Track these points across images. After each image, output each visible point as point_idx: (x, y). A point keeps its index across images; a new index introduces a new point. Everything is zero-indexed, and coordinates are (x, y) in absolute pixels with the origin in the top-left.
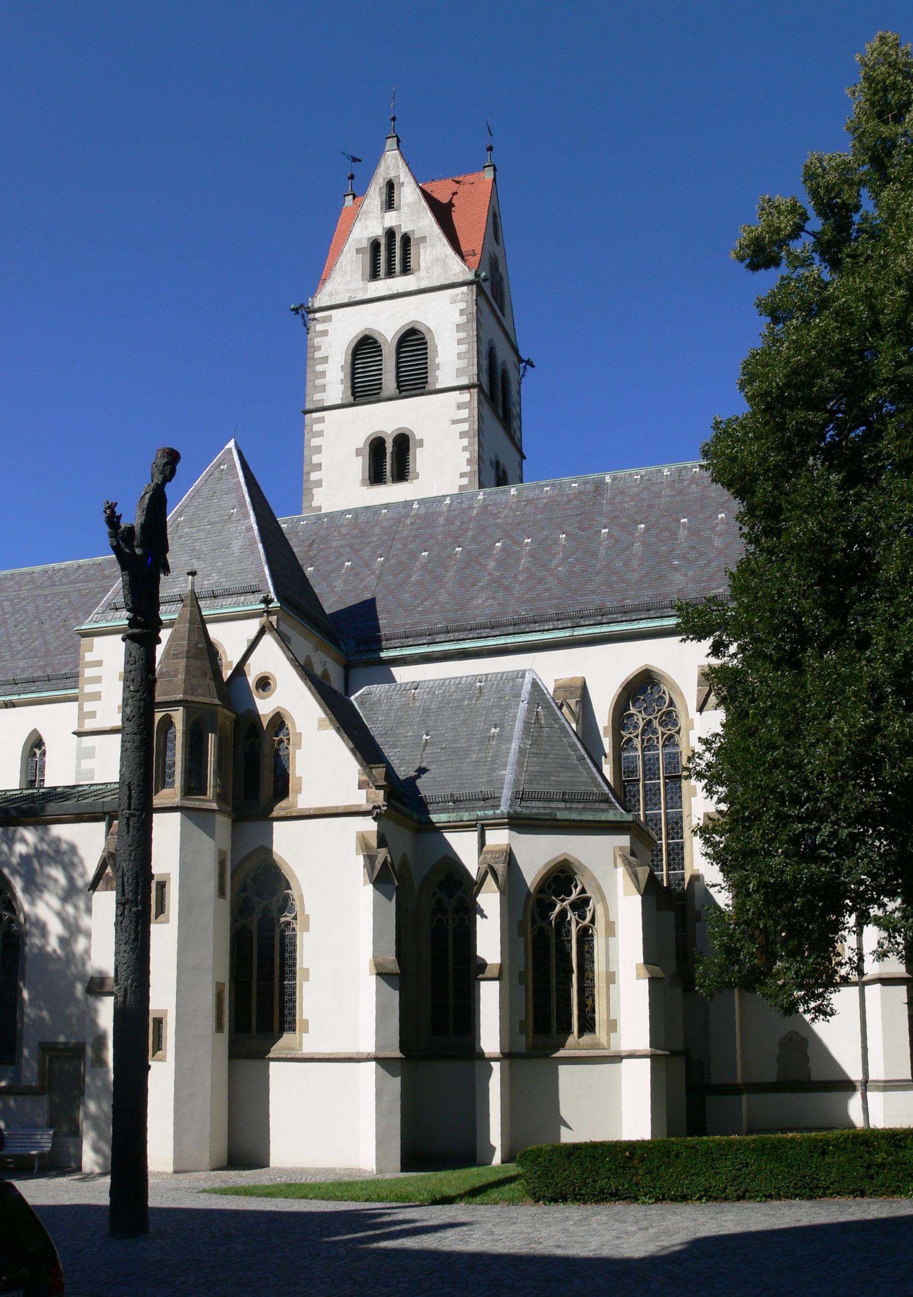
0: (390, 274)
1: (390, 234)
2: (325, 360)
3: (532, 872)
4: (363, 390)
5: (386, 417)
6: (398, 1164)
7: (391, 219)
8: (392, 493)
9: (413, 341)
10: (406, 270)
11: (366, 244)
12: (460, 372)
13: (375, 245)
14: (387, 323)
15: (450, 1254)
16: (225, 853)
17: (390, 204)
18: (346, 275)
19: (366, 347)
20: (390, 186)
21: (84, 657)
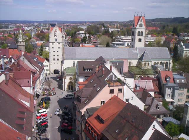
1: (141, 24)
4: (139, 35)
5: (140, 37)
6: (124, 62)
7: (141, 23)
8: (112, 88)
10: (142, 27)
13: (140, 24)
14: (141, 31)
15: (150, 126)
17: (141, 21)
18: (138, 27)
19: (139, 32)
21: (79, 80)
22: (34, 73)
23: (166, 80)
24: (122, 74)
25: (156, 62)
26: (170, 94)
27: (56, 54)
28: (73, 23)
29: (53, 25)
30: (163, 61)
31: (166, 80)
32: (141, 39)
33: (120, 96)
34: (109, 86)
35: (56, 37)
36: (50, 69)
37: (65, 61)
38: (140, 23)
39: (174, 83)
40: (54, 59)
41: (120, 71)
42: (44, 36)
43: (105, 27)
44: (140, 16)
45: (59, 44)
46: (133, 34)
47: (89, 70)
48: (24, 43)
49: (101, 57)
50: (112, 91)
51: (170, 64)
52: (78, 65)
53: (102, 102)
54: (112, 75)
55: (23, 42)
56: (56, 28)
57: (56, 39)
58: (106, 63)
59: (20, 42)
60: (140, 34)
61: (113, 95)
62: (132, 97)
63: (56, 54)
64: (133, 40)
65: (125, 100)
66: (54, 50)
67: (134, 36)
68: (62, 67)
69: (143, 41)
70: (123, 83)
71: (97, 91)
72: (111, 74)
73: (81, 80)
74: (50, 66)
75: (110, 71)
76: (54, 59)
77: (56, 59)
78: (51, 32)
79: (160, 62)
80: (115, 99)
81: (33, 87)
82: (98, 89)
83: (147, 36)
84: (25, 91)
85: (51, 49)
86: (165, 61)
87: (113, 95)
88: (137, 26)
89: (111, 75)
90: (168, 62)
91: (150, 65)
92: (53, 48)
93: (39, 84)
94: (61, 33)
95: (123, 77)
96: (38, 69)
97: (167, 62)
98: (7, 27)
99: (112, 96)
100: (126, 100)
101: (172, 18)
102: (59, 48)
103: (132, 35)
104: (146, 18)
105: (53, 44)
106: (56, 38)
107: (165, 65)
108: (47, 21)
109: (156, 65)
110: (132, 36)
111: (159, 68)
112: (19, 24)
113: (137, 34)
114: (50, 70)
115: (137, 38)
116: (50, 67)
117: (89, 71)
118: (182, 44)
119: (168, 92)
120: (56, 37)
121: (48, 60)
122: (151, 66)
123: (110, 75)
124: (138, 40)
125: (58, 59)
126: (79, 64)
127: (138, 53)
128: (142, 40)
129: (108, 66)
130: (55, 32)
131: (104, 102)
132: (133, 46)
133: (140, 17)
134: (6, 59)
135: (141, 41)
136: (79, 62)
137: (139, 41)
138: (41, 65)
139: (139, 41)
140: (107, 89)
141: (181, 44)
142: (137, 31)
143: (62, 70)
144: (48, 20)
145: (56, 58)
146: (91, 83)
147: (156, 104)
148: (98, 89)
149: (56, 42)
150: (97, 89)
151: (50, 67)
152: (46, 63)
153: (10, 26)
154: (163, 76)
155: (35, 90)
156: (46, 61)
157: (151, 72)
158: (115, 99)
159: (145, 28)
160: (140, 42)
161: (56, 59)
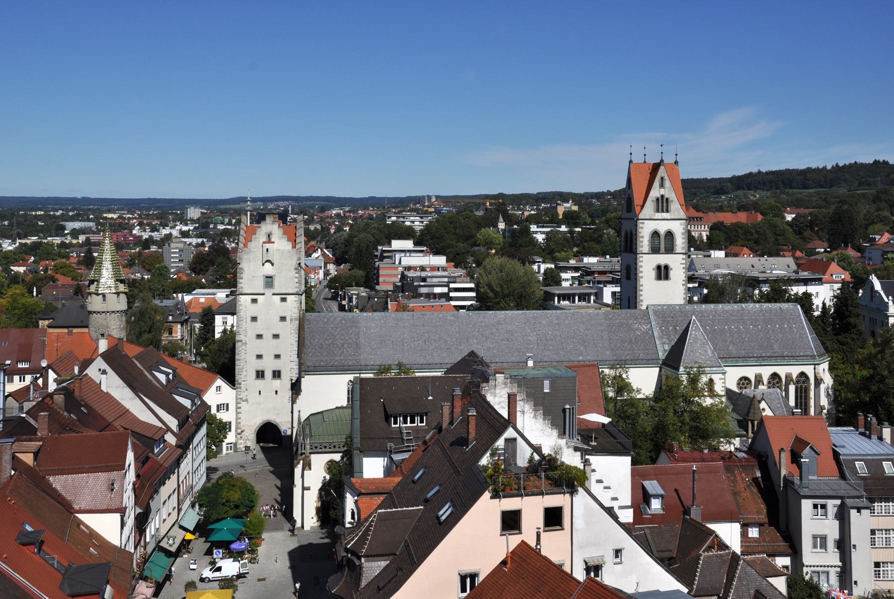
0: (663, 211)
2: (643, 237)
3: (663, 456)
4: (655, 250)
5: (662, 259)
7: (662, 192)
9: (670, 235)
10: (667, 211)
11: (654, 199)
12: (683, 248)
13: (658, 199)
14: (663, 227)
16: (8, 382)
17: (662, 186)
18: (649, 210)
19: (655, 234)
20: (662, 178)
22: (147, 440)
23: (795, 458)
24: (571, 436)
25: (750, 372)
26: (824, 539)
27: (268, 347)
28: (366, 208)
29: (260, 218)
30: (782, 371)
31: (795, 458)
32: (667, 267)
33: (554, 547)
34: (496, 495)
35: (268, 269)
36: (237, 423)
37: (307, 382)
38: (655, 193)
39: (843, 476)
40: (258, 372)
41: (560, 419)
42: (217, 265)
43: (509, 220)
44: (653, 160)
45: (284, 300)
46: (628, 246)
47: (412, 421)
48: (123, 298)
49: (472, 354)
50: (511, 522)
51: (818, 381)
52: (357, 396)
53: (463, 579)
54: (511, 441)
55: (118, 294)
56: (271, 226)
57: (269, 281)
58: (491, 383)
59: (104, 295)
60: (663, 243)
61: (514, 541)
62: (618, 552)
63: (268, 347)
64: (628, 278)
65: (580, 575)
66: (258, 328)
67: (633, 255)
68: (292, 412)
69: (678, 273)
70: (570, 481)
71: (440, 523)
72: (510, 433)
73: (373, 468)
74: (237, 408)
75: (510, 422)
76: (258, 372)
77: (268, 374)
78: (245, 246)
79: (766, 372)
80: (525, 564)
81: (139, 510)
82: (445, 512)
83: (709, 256)
84: (93, 535)
85: (248, 325)
86: (795, 371)
87: (514, 541)
88: (642, 207)
89: (506, 440)
90: (809, 370)
91: (719, 388)
92: (254, 319)
93: (175, 497)
94: (294, 247)
95: (576, 449)
96: (173, 423)
97: (802, 374)
98: (59, 230)
99: (510, 550)
100: (588, 569)
101: (829, 167)
102: (283, 319)
103: (626, 251)
104: (687, 173)
105: (254, 301)
106: (269, 273)
107: (792, 388)
108: (244, 200)
109: (749, 392)
110: (625, 255)
111: (763, 405)
112: (115, 216)
113: (644, 243)
114: (237, 428)
115: (647, 263)
116: (242, 407)
117: (409, 425)
118: (877, 286)
119: (815, 523)
120: (268, 269)
121: (230, 378)
122: (723, 393)
123: (500, 443)
124: (653, 274)
125: (277, 374)
126: (361, 389)
127: (656, 334)
128: (672, 274)
129: (497, 398)
130: (267, 246)
131: (473, 576)
132: (628, 299)
133: (656, 167)
134: (16, 378)
135: (667, 277)
136: (362, 380)
137: (659, 277)
138: (187, 403)
139: (659, 277)
140: (487, 510)
141: (873, 287)
142: (645, 230)
143: (295, 424)
144: (249, 194)
145: (269, 364)
146: (414, 482)
147: (752, 592)
148: (445, 512)
149: (269, 292)
150: (441, 513)
151: (242, 407)
152: (217, 395)
153: (71, 225)
154: (779, 443)
155: (150, 531)
156: (219, 382)
157: (731, 421)
158: (525, 564)
159: (683, 215)
160: (663, 283)
161: (268, 374)
